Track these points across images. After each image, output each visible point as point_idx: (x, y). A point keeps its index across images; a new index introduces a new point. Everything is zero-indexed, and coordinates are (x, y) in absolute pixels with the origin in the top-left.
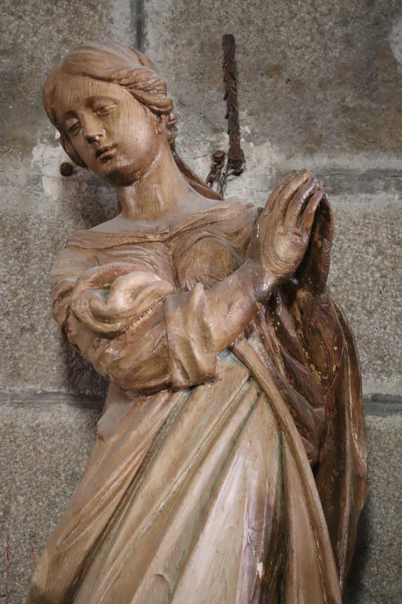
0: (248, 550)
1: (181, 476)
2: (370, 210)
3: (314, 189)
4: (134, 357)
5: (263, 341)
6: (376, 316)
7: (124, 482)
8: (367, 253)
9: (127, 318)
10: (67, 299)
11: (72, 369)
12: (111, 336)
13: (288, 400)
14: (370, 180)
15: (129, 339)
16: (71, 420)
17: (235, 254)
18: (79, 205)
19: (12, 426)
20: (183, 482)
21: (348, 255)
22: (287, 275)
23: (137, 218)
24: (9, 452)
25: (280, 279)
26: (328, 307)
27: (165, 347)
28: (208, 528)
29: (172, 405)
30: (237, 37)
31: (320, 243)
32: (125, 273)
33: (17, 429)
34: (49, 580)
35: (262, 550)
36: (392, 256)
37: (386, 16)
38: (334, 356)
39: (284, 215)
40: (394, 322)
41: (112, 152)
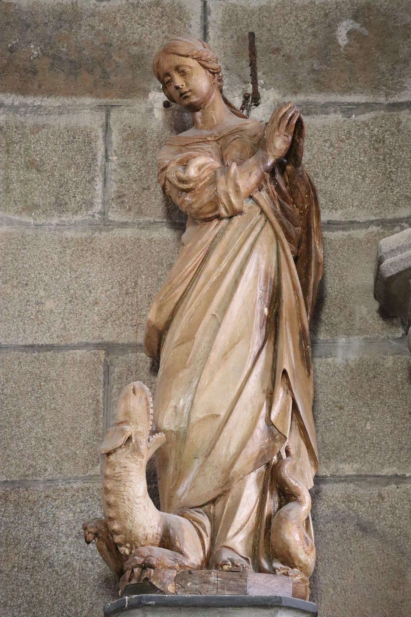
0: (260, 301)
1: (224, 264)
2: (326, 124)
3: (295, 112)
4: (200, 201)
5: (268, 193)
6: (329, 179)
7: (195, 267)
8: (325, 146)
9: (196, 181)
10: (165, 172)
11: (169, 210)
12: (187, 191)
13: (281, 224)
14: (326, 107)
15: (197, 192)
16: (169, 236)
17: (253, 146)
18: (173, 123)
19: (138, 239)
20: (225, 267)
21: (315, 147)
22: (281, 157)
23: (202, 129)
24: (137, 252)
25: (277, 160)
26: (303, 174)
27: (216, 196)
28: (239, 290)
29: (220, 227)
30: (256, 34)
31: (298, 140)
32: (195, 157)
33: (141, 241)
34: (156, 317)
35: (267, 301)
36: (338, 147)
37: (334, 22)
38: (305, 200)
39: (279, 126)
40: (339, 182)
41: (189, 94)
